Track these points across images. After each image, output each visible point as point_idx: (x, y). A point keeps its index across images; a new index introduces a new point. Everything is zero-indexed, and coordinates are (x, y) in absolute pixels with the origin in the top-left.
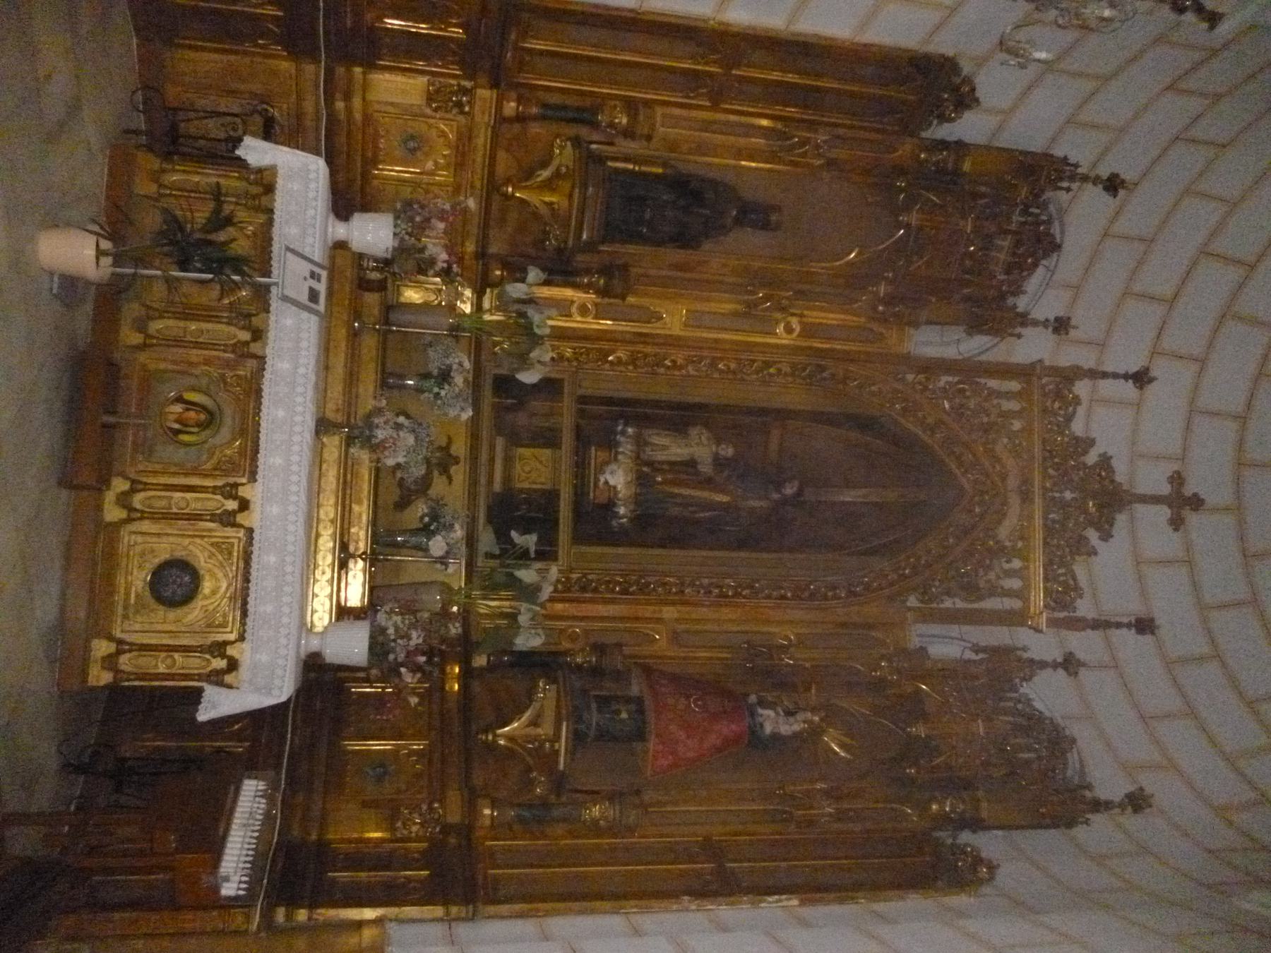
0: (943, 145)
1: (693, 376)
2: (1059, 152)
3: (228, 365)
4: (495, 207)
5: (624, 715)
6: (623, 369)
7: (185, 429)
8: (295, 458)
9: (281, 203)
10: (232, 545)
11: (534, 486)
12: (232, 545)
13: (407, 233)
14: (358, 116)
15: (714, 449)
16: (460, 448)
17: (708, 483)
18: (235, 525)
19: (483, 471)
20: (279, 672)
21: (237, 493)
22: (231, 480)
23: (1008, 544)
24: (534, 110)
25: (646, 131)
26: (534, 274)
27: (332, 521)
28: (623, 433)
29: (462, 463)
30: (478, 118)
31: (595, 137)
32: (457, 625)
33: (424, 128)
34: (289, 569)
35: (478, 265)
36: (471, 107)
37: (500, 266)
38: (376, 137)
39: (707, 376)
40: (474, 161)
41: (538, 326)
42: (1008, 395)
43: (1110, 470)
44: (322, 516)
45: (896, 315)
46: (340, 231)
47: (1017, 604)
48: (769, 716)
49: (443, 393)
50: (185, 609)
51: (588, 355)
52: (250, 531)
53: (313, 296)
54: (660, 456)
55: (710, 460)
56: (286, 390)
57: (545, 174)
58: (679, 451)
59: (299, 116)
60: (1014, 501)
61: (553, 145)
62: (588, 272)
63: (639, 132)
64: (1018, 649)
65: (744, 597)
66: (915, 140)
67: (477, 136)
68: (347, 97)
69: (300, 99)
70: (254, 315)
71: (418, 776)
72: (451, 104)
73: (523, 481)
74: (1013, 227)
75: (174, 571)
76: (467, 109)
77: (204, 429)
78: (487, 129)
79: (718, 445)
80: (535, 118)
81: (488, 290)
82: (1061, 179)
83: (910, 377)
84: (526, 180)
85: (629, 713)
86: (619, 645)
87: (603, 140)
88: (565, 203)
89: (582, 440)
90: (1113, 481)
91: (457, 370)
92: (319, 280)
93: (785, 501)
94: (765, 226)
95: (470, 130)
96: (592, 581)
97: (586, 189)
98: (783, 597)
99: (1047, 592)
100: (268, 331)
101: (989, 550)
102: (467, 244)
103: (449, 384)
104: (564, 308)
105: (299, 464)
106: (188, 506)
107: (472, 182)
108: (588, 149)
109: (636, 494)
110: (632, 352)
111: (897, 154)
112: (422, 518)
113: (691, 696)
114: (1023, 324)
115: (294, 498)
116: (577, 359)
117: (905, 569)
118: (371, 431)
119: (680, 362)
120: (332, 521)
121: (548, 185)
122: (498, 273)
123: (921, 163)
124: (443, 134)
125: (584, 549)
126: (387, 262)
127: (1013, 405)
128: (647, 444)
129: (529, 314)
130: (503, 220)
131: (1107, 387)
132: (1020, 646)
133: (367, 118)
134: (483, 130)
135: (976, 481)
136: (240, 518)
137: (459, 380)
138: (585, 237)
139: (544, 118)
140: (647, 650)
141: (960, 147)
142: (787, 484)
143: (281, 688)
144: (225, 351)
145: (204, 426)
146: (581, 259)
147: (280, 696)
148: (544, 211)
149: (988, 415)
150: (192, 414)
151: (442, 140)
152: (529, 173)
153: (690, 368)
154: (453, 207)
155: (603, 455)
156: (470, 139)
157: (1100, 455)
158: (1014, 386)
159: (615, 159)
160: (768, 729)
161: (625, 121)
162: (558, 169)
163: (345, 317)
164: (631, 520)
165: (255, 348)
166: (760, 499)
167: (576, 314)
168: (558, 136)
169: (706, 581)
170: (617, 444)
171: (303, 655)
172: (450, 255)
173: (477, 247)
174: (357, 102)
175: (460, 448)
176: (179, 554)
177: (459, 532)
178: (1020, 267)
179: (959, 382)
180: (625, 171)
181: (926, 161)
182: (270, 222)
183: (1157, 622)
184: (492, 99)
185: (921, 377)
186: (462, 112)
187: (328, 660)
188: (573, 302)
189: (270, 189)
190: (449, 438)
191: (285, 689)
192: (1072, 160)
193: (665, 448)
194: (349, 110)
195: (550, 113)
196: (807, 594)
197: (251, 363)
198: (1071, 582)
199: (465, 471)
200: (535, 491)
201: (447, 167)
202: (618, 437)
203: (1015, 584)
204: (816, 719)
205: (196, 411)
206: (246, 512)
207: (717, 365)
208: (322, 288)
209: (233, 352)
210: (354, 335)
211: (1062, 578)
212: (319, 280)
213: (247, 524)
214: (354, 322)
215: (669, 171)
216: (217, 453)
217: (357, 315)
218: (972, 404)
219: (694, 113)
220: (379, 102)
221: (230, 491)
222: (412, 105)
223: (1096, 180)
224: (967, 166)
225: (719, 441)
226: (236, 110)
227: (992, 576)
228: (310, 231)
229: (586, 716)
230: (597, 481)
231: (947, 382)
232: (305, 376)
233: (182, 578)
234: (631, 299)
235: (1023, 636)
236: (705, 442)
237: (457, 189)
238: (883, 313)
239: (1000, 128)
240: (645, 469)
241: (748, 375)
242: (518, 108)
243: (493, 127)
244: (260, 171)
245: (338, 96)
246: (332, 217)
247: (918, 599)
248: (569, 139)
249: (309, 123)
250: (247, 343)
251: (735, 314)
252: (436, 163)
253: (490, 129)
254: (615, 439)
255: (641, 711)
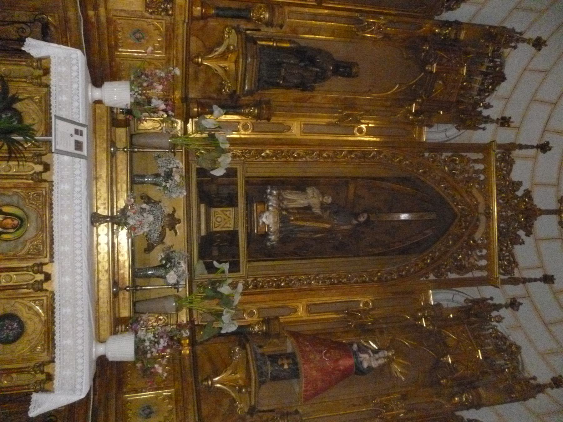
0: (447, 24)
1: (310, 161)
2: (509, 25)
3: (29, 187)
4: (191, 70)
5: (286, 367)
6: (270, 160)
7: (5, 231)
8: (78, 246)
9: (54, 80)
10: (43, 300)
11: (224, 229)
12: (43, 300)
13: (138, 94)
14: (103, 19)
15: (321, 199)
16: (180, 214)
17: (318, 218)
18: (42, 290)
19: (195, 223)
20: (79, 380)
21: (42, 269)
22: (38, 261)
23: (480, 242)
24: (212, 12)
25: (280, 22)
26: (217, 110)
27: (106, 271)
28: (271, 194)
29: (182, 222)
30: (178, 18)
31: (250, 26)
32: (187, 331)
33: (145, 24)
34: (79, 316)
35: (183, 106)
36: (173, 11)
37: (196, 106)
38: (116, 31)
39: (317, 161)
40: (177, 43)
41: (222, 143)
42: (477, 161)
43: (530, 198)
44: (100, 268)
45: (419, 121)
46: (97, 93)
47: (485, 274)
48: (365, 358)
49: (168, 185)
50: (16, 343)
51: (250, 153)
52: (53, 293)
53: (78, 146)
54: (292, 205)
55: (319, 205)
56: (68, 202)
57: (221, 49)
58: (302, 202)
59: (66, 20)
60: (483, 218)
61: (223, 32)
62: (248, 106)
63: (275, 23)
64: (487, 299)
65: (343, 283)
66: (432, 21)
67: (178, 28)
68: (95, 8)
69: (65, 11)
70: (44, 155)
71: (170, 411)
72: (160, 9)
73: (217, 227)
74: (484, 69)
75: (7, 322)
76: (170, 12)
77: (18, 230)
78: (183, 24)
79: (323, 197)
80: (211, 16)
81: (190, 120)
82: (512, 42)
83: (427, 154)
84: (210, 54)
85: (288, 364)
86: (277, 318)
87: (254, 28)
88: (233, 66)
89: (249, 201)
90: (532, 204)
91: (176, 171)
92: (81, 135)
93: (359, 224)
94: (349, 75)
95: (174, 24)
96: (260, 282)
97: (247, 59)
98: (364, 282)
99: (500, 266)
100: (53, 165)
101: (471, 245)
102: (176, 93)
103: (172, 180)
104: (233, 126)
105: (80, 249)
106: (11, 280)
107: (177, 57)
108: (246, 34)
109: (280, 227)
110: (275, 150)
111: (422, 30)
112: (161, 261)
113: (322, 352)
114: (486, 122)
115: (79, 271)
116: (244, 156)
117: (427, 260)
118: (126, 219)
119: (302, 153)
120: (106, 271)
121: (223, 56)
122: (196, 110)
123: (435, 34)
124: (157, 28)
125: (256, 264)
126: (129, 112)
127: (481, 167)
128: (284, 199)
129: (216, 136)
130: (196, 78)
131: (524, 152)
132: (489, 297)
133: (109, 21)
134: (181, 25)
135: (463, 209)
136: (45, 286)
137: (177, 178)
138: (246, 88)
139: (218, 16)
140: (293, 317)
141: (457, 24)
142: (361, 215)
143: (81, 390)
144: (27, 179)
145: (17, 228)
146: (245, 100)
147: (81, 395)
148: (220, 71)
149: (468, 173)
150: (9, 221)
151: (157, 32)
152: (211, 50)
153: (307, 157)
154: (166, 74)
155: (260, 207)
156: (174, 31)
157: (525, 191)
158: (480, 156)
159: (262, 40)
160: (365, 365)
161: (267, 16)
162: (228, 48)
163: (105, 146)
164: (277, 241)
165: (45, 176)
166: (347, 225)
167: (242, 130)
168: (226, 26)
169: (322, 276)
170: (268, 200)
171: (94, 357)
172: (167, 105)
173: (182, 94)
174: (102, 11)
175: (180, 214)
176: (9, 310)
177: (183, 266)
178: (485, 91)
179: (452, 156)
180: (269, 47)
181: (439, 34)
182: (49, 94)
183: (555, 277)
184: (185, 5)
185: (433, 154)
186: (168, 15)
187: (111, 359)
188: (239, 123)
189: (47, 72)
190: (174, 208)
191: (83, 390)
192: (517, 30)
193: (294, 201)
194: (97, 15)
195: (221, 13)
196: (376, 279)
197: (46, 185)
198: (512, 259)
199: (186, 313)
200: (225, 232)
201: (160, 48)
202: (268, 196)
203: (483, 263)
204: (390, 354)
205: (12, 219)
206: (49, 281)
207: (322, 154)
208: (84, 139)
209: (32, 179)
210: (112, 156)
211: (507, 258)
212: (81, 135)
213: (50, 289)
214: (111, 148)
215: (293, 45)
216: (28, 244)
217: (113, 143)
218: (459, 167)
219: (307, 10)
220: (116, 10)
221: (39, 268)
222: (136, 11)
223: (528, 41)
224: (462, 36)
225: (323, 194)
226: (25, 19)
227: (472, 260)
228: (76, 98)
229: (265, 368)
230: (258, 222)
231: (447, 156)
232: (79, 192)
233: (12, 325)
234: (274, 120)
235: (487, 292)
236: (316, 196)
237: (168, 61)
238: (412, 120)
239: (477, 13)
240: (284, 213)
241: (340, 159)
242: (202, 11)
243: (188, 23)
244: (40, 60)
245: (89, 7)
246: (90, 86)
247: (434, 275)
248: (233, 28)
249: (72, 25)
250: (41, 173)
251: (328, 124)
252: (154, 46)
253: (185, 24)
254: (266, 198)
255: (296, 363)
